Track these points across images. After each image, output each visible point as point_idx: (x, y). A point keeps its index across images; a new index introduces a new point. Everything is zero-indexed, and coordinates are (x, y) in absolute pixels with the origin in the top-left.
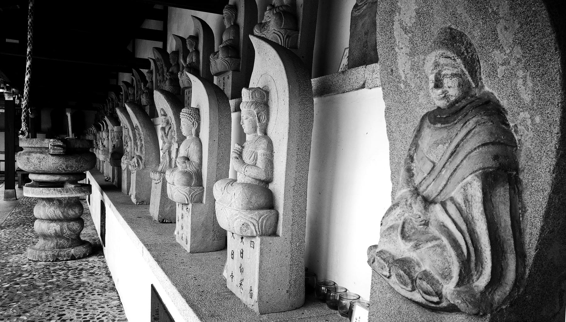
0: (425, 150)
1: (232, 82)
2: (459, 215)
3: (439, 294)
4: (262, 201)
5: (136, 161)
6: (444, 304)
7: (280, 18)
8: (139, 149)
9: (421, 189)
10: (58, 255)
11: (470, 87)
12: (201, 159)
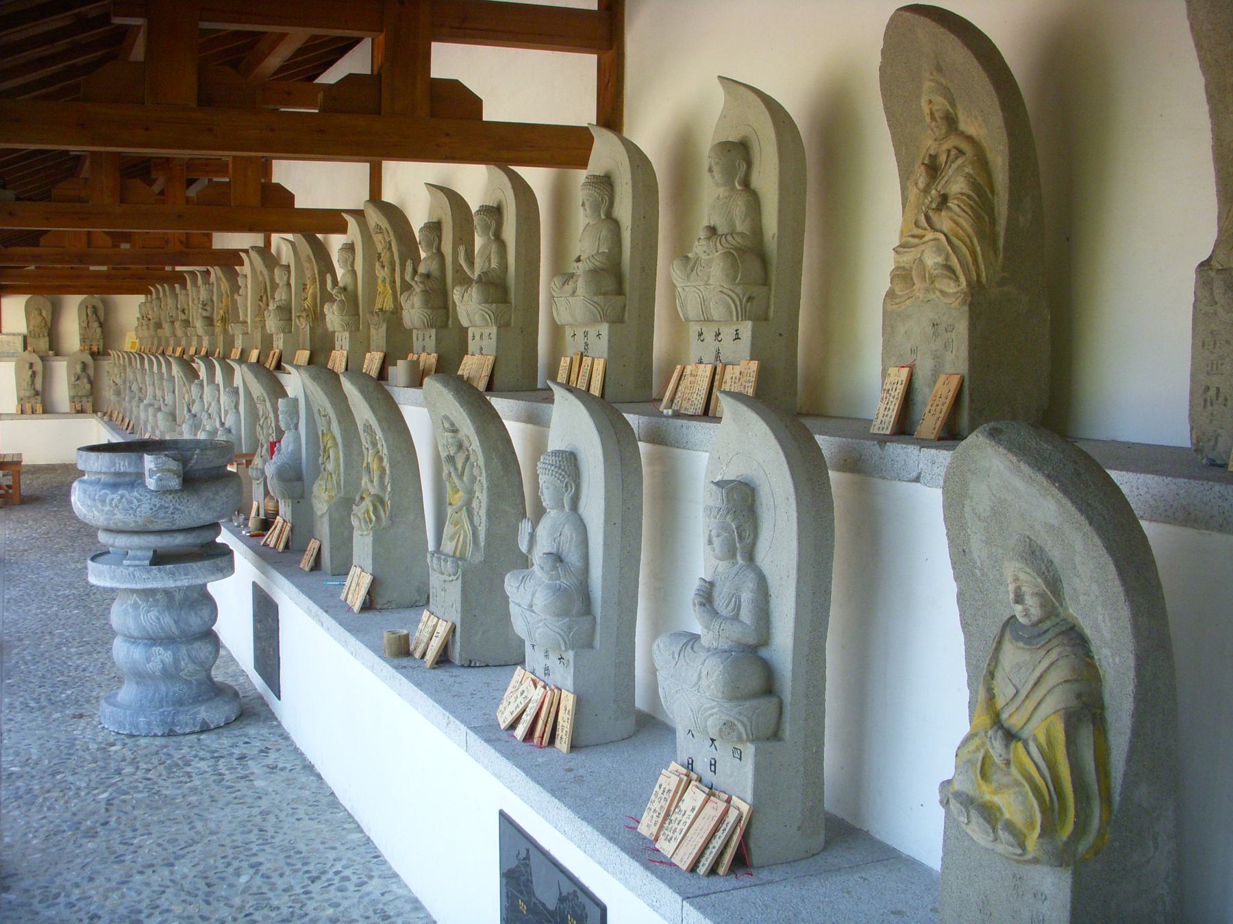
0: (1007, 670)
4: (754, 681)
5: (371, 509)
6: (1028, 857)
7: (734, 265)
8: (376, 479)
9: (1004, 716)
11: (1054, 606)
12: (586, 558)
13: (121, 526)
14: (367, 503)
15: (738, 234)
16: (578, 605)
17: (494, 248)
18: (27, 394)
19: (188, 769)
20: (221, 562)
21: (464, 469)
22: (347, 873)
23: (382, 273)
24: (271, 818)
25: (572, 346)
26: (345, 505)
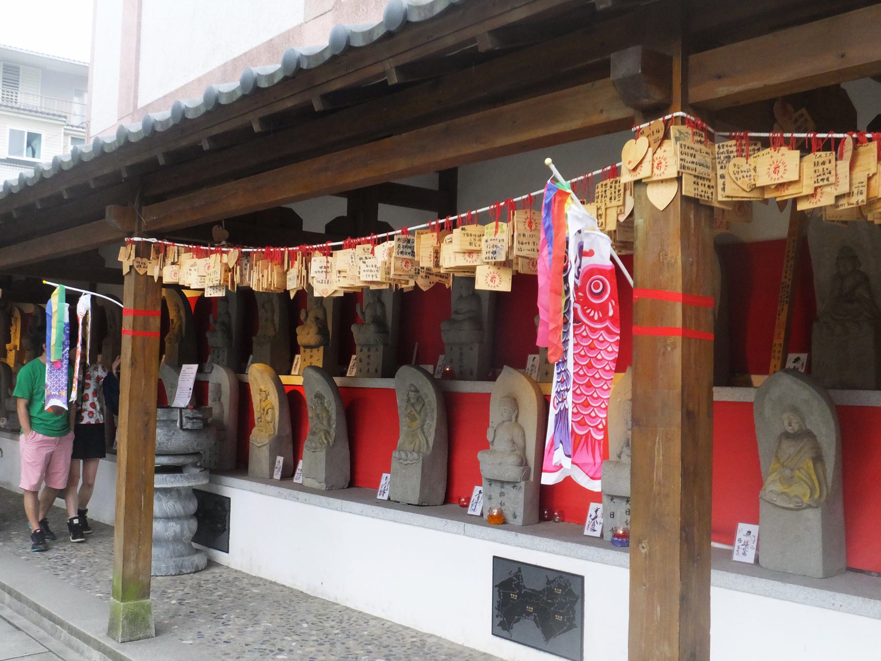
2: (171, 458)
3: (802, 502)
10: (182, 567)
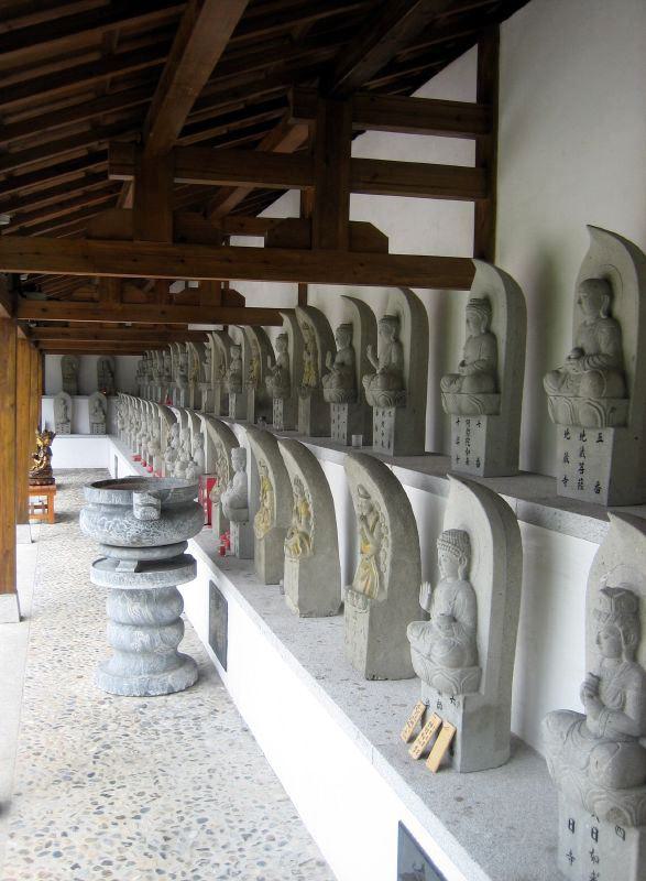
1: (488, 435)
13: (114, 543)
14: (296, 538)
15: (604, 355)
16: (468, 659)
17: (394, 348)
18: (62, 421)
19: (156, 727)
20: (186, 570)
21: (374, 527)
22: (272, 832)
23: (307, 358)
24: (216, 775)
25: (456, 431)
26: (280, 533)
